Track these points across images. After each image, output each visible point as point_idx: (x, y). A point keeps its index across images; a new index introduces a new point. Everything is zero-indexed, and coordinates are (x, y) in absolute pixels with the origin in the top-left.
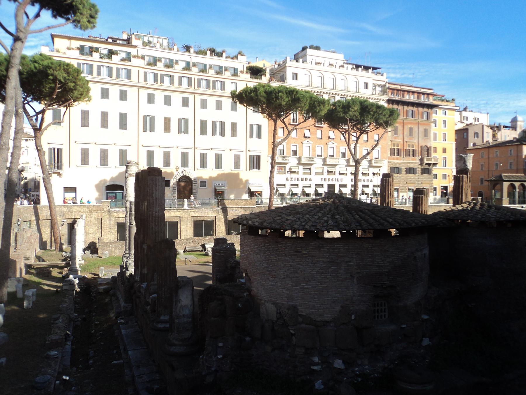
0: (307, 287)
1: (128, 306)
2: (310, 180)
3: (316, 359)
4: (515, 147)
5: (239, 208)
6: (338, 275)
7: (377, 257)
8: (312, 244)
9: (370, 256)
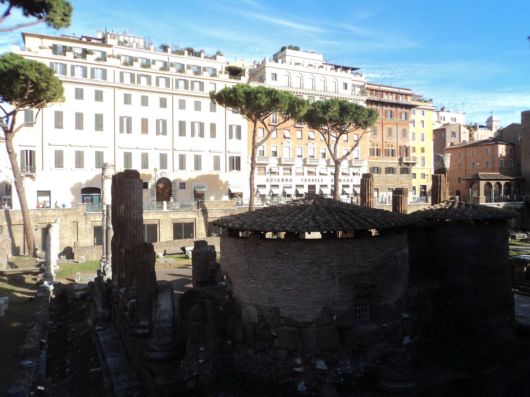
0: (288, 288)
1: (106, 311)
2: (291, 180)
3: (299, 361)
4: (491, 146)
5: (220, 210)
6: (319, 276)
7: (358, 257)
8: (294, 245)
9: (351, 256)
